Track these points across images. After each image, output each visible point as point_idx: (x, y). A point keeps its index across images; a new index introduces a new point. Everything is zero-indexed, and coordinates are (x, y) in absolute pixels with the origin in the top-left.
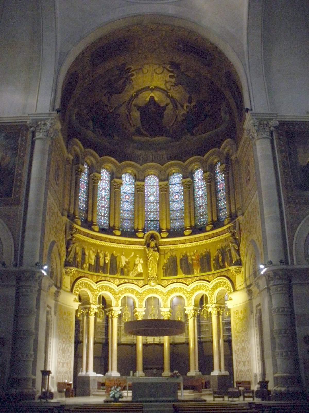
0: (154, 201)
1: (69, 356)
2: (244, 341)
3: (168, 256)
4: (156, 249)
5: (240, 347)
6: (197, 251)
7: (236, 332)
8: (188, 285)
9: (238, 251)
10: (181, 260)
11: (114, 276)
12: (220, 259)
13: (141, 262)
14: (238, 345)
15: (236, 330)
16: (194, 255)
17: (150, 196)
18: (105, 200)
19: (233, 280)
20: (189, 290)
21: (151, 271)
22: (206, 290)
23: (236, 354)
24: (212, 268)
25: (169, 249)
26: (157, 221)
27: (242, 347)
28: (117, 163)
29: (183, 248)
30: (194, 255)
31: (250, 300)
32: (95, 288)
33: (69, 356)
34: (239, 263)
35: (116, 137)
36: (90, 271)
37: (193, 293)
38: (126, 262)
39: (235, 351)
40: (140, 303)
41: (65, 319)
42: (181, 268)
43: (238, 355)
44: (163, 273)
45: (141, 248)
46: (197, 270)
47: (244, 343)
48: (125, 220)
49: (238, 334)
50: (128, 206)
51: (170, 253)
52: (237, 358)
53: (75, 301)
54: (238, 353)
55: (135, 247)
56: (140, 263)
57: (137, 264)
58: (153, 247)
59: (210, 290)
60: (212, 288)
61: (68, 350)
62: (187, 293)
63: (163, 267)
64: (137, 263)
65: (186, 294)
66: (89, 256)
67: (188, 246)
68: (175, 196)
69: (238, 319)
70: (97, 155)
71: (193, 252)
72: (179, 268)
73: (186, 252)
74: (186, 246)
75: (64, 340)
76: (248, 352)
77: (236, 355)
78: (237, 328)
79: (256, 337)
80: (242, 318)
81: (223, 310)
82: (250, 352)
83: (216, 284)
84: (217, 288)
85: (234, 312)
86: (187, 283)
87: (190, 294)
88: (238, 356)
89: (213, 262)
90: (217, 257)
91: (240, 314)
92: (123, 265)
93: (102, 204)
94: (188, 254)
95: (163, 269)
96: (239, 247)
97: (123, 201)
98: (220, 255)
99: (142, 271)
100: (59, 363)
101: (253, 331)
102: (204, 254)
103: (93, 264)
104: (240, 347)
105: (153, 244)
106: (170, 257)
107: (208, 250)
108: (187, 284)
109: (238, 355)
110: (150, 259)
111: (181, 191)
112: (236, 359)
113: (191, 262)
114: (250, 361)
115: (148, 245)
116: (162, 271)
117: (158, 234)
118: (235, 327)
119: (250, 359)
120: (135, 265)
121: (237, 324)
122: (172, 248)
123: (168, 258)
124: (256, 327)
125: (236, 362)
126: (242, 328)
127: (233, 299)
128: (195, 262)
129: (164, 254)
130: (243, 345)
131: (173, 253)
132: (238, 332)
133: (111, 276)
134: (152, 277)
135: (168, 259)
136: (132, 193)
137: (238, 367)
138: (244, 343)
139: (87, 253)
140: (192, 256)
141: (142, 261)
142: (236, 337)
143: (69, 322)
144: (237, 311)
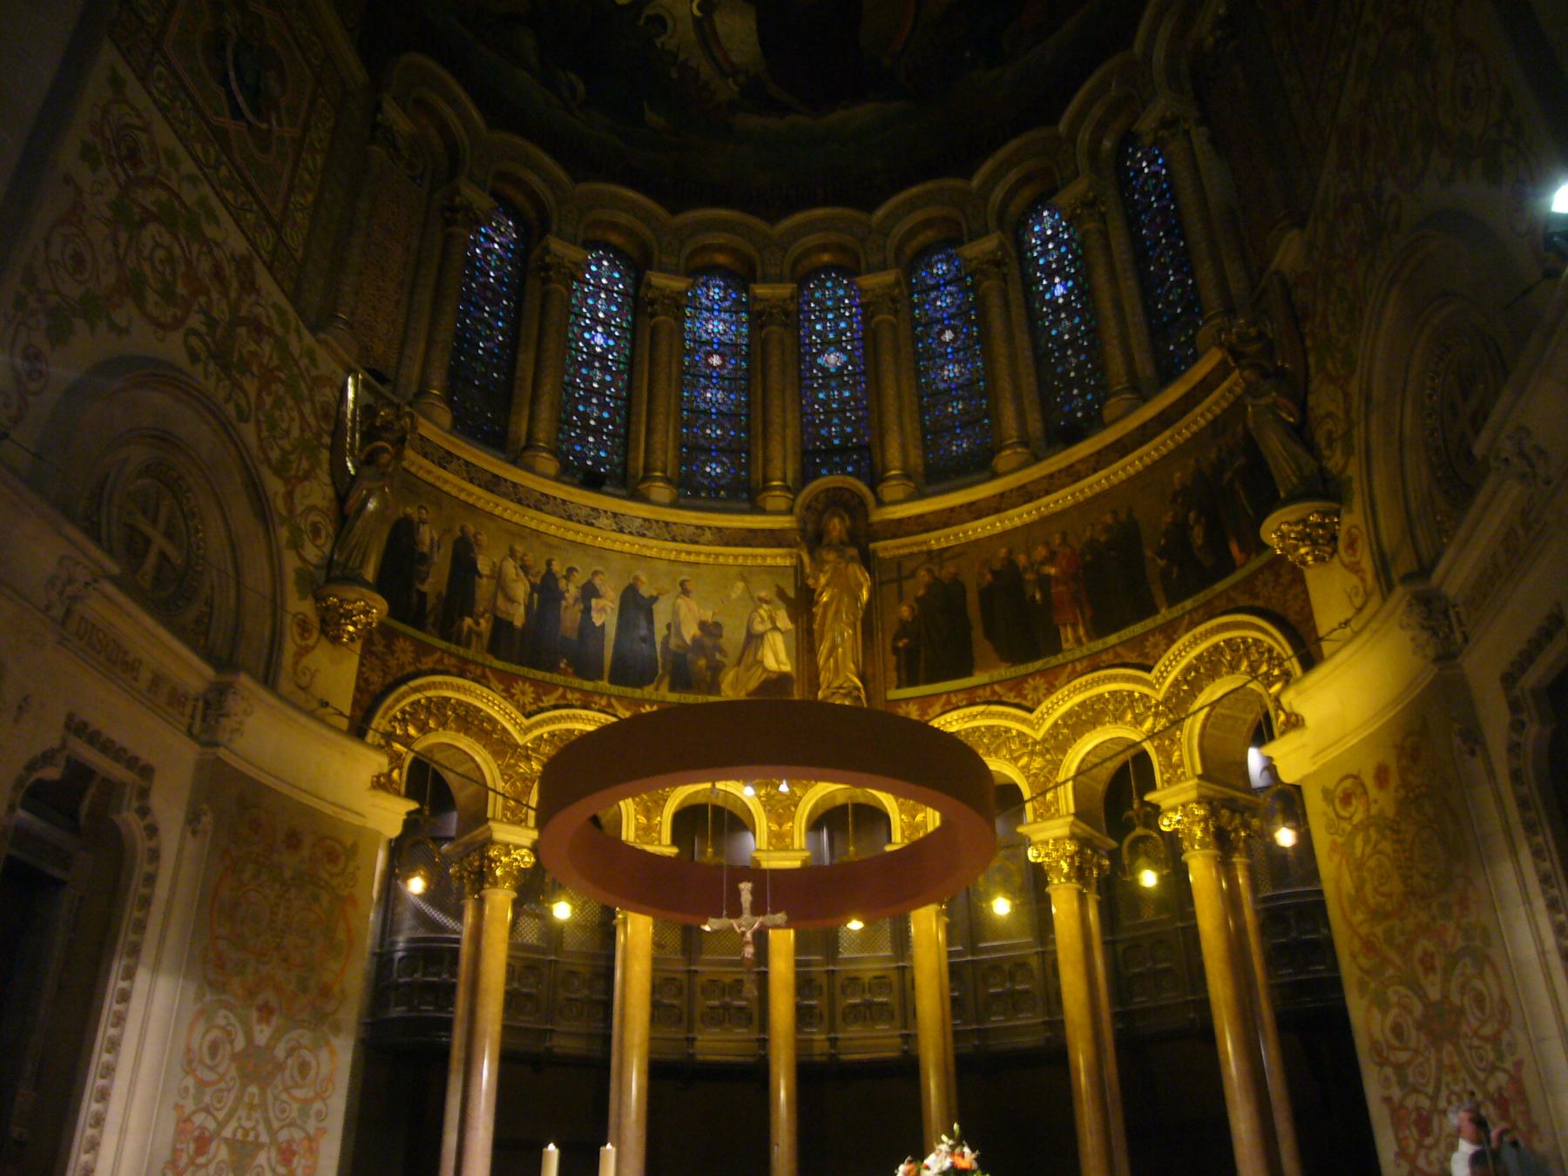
0: (844, 366)
1: (306, 1102)
2: (1438, 963)
3: (918, 586)
4: (853, 552)
5: (1406, 1009)
6: (1064, 535)
7: (1359, 917)
8: (1031, 711)
9: (1301, 432)
10: (986, 595)
11: (638, 693)
12: (1198, 536)
13: (779, 625)
14: (1393, 999)
15: (1358, 899)
16: (1051, 558)
17: (821, 353)
18: (605, 369)
19: (1292, 617)
20: (1039, 736)
21: (827, 659)
22: (1135, 717)
23: (1381, 1065)
24: (1159, 597)
25: (921, 553)
26: (856, 449)
27: (1427, 1005)
28: (660, 212)
29: (990, 538)
30: (1051, 558)
31: (1446, 656)
32: (521, 742)
33: (306, 1102)
34: (1325, 488)
35: (653, 118)
36: (497, 657)
37: (1063, 748)
38: (703, 625)
39: (1375, 1046)
40: (775, 827)
41: (288, 874)
42: (989, 633)
43: (1399, 1068)
44: (898, 669)
45: (780, 562)
46: (1074, 626)
47: (1436, 978)
48: (708, 451)
49: (1379, 930)
50: (720, 395)
51: (929, 571)
52: (1396, 1093)
53: (382, 784)
54: (1403, 1056)
55: (745, 556)
56: (775, 628)
57: (761, 636)
58: (840, 547)
59: (1156, 715)
60: (1166, 700)
61: (304, 1067)
62: (1032, 753)
63: (896, 638)
64: (759, 627)
65: (1024, 761)
66: (498, 576)
67: (1017, 522)
68: (942, 332)
69: (1364, 826)
70: (562, 175)
71: (1047, 544)
72: (977, 633)
73: (1010, 552)
74: (1008, 525)
75: (268, 995)
76: (1488, 1030)
77: (1389, 1071)
78: (1368, 888)
79: (1540, 904)
80: (1390, 812)
81: (1246, 826)
82: (1505, 1024)
83: (1188, 669)
84: (1196, 688)
85: (1327, 795)
86: (1024, 703)
87: (1042, 754)
88: (1403, 1083)
89: (1155, 564)
90: (1180, 531)
91: (1373, 792)
92: (688, 640)
93: (592, 381)
94: (1022, 559)
95: (895, 650)
96: (1303, 408)
97: (694, 375)
98: (1192, 515)
99: (787, 668)
100: (202, 1143)
101: (1506, 870)
102: (1103, 539)
103: (519, 622)
104: (1406, 1009)
105: (837, 526)
106: (929, 587)
107: (1123, 517)
108: (1028, 704)
109: (1399, 1068)
110: (825, 598)
111: (964, 308)
112: (1387, 1100)
113: (1038, 596)
114: (1521, 1093)
115: (814, 540)
116: (892, 660)
117: (862, 488)
118: (1348, 885)
119: (1516, 1081)
120: (754, 639)
121: (1359, 866)
122: (934, 545)
123: (921, 592)
124: (1530, 828)
125: (1397, 1122)
126: (1405, 879)
127: (1309, 722)
128: (1059, 590)
129: (899, 580)
130: (1434, 994)
131: (941, 568)
132: (1377, 915)
133: (615, 689)
134: (836, 684)
135: (918, 600)
136: (736, 345)
137: (1412, 1160)
138: (1436, 978)
139: (483, 565)
140: (1043, 563)
141: (784, 621)
142: (1369, 946)
143: (325, 899)
144: (1348, 783)
